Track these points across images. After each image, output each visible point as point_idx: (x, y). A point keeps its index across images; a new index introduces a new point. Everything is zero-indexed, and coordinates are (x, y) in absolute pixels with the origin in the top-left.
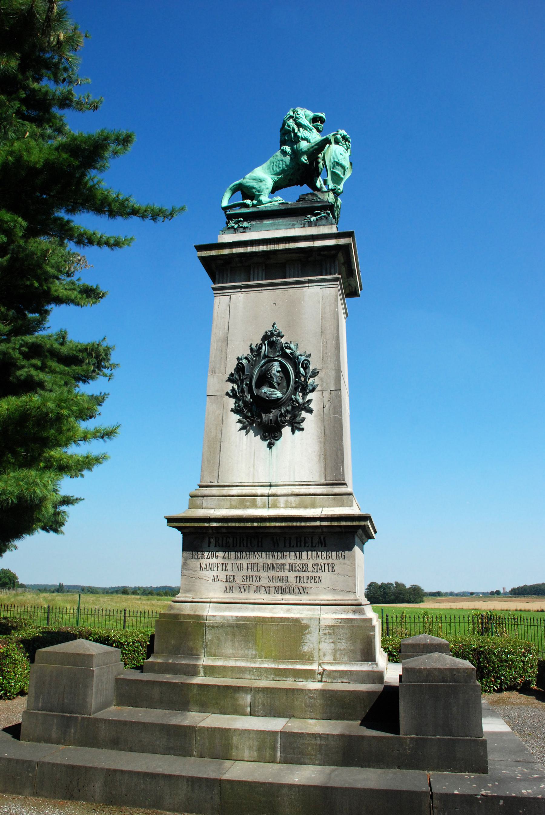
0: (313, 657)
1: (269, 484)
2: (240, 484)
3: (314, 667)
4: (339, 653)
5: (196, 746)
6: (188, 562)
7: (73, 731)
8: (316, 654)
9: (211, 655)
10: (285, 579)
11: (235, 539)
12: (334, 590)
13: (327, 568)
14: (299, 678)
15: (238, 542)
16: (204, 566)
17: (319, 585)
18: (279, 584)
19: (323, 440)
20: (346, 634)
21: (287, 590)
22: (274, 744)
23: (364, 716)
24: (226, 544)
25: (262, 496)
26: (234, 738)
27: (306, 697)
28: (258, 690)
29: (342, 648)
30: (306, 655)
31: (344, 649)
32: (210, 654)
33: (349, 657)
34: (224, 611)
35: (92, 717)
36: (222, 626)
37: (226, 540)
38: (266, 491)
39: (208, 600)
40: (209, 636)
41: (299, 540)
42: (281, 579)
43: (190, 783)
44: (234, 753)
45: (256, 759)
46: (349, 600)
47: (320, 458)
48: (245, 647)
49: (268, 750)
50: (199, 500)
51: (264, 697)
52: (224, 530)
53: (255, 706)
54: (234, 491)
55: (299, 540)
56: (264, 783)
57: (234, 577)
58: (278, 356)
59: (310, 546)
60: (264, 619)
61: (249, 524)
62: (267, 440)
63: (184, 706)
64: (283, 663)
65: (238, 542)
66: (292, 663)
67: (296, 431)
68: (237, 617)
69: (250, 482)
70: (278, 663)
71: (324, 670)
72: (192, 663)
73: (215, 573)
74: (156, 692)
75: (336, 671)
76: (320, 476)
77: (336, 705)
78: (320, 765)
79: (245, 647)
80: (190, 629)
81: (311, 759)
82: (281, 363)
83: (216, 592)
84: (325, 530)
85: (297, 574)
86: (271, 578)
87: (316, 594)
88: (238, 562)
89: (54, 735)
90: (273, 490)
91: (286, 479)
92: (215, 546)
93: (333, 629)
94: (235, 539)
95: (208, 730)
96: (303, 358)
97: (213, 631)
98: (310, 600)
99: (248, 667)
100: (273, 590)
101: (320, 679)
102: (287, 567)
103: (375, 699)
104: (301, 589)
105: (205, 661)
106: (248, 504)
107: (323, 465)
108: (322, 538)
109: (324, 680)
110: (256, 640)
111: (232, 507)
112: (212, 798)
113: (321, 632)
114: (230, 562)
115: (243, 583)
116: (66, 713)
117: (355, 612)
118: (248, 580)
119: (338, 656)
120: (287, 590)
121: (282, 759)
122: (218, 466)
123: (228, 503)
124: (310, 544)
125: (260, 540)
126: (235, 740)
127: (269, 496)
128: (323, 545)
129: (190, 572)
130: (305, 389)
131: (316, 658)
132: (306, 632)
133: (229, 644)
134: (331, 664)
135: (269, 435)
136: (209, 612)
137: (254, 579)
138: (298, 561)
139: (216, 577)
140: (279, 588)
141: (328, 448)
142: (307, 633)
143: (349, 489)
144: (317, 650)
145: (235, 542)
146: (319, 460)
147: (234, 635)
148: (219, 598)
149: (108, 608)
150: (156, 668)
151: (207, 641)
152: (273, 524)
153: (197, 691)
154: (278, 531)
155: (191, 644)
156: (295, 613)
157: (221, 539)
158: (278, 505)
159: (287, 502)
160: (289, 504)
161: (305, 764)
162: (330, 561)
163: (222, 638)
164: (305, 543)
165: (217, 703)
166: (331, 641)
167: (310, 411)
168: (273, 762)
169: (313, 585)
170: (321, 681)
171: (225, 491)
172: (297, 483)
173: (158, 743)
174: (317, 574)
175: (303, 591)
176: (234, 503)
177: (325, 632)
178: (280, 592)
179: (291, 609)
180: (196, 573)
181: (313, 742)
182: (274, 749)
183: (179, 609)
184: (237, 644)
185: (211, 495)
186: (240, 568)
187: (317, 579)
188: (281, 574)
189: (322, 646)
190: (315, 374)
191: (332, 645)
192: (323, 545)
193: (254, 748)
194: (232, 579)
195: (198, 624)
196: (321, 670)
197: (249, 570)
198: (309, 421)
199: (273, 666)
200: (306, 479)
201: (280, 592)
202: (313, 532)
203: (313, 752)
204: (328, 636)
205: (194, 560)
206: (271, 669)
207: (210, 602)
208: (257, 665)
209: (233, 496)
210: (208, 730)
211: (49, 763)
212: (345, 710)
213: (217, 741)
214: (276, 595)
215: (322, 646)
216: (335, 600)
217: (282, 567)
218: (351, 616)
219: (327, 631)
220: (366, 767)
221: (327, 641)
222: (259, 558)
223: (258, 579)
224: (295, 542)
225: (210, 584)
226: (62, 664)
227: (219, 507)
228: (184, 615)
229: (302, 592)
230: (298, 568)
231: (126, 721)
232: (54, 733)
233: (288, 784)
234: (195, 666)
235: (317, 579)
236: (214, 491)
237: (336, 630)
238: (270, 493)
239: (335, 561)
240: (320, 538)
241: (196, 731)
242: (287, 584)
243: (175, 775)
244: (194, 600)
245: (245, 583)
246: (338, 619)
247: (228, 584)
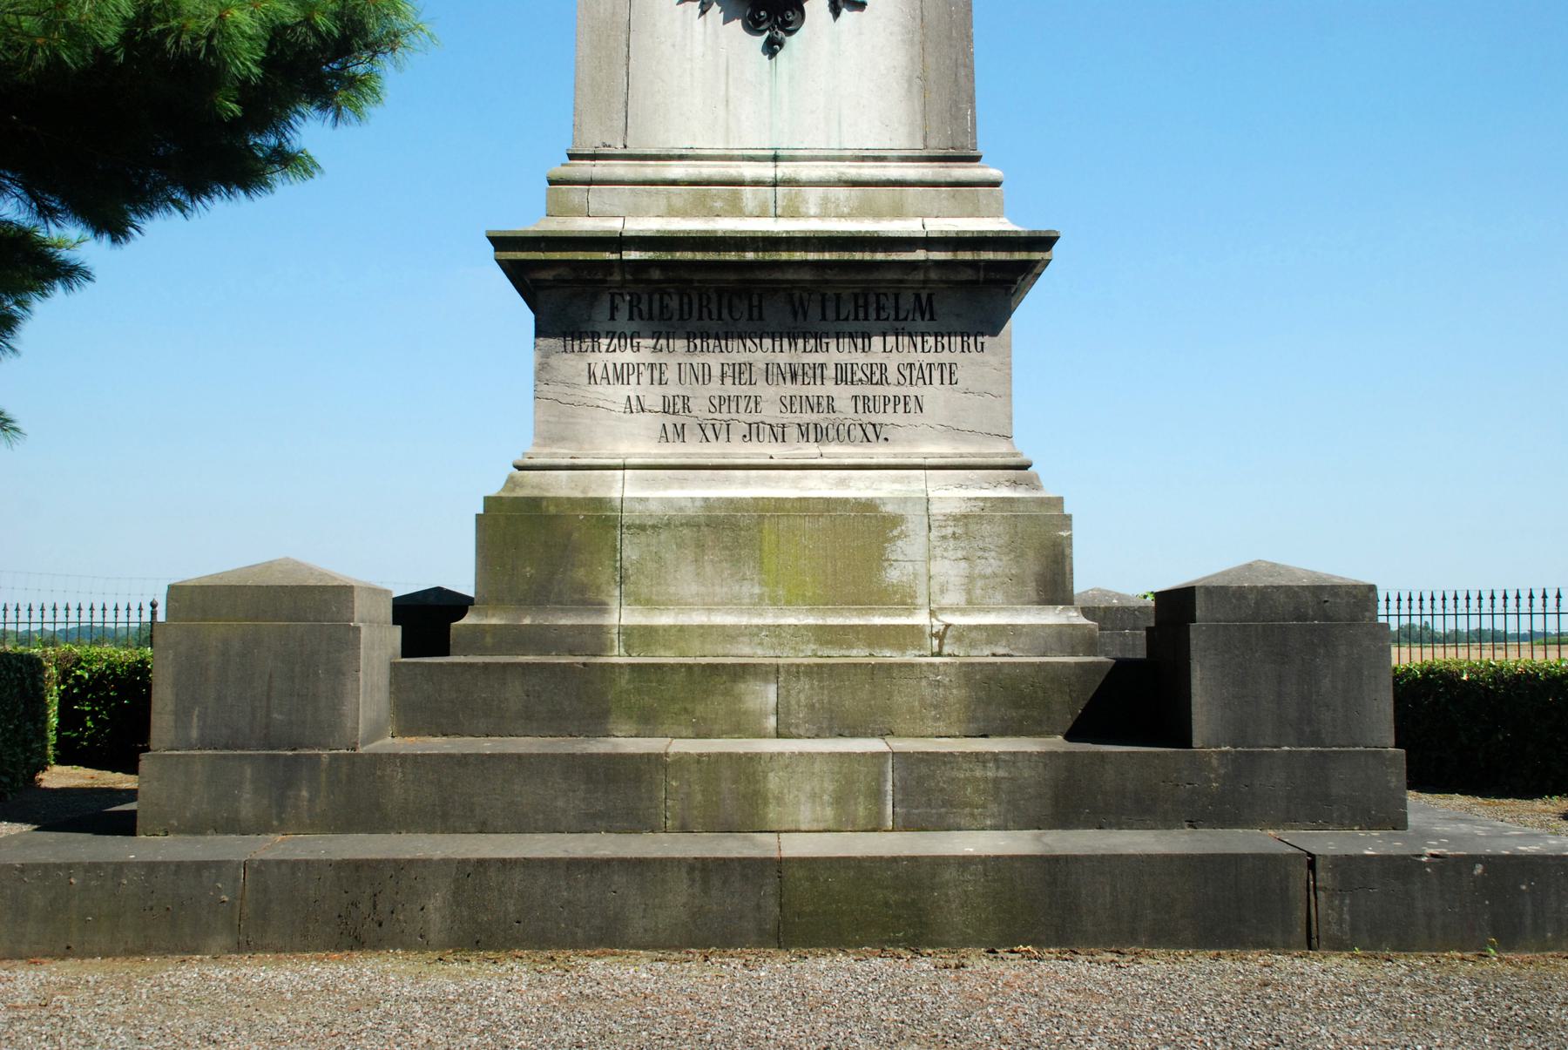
0: (913, 597)
1: (772, 153)
2: (690, 152)
3: (921, 619)
4: (980, 583)
5: (669, 803)
6: (553, 360)
7: (305, 793)
8: (921, 590)
9: (638, 601)
10: (824, 403)
11: (686, 300)
12: (954, 431)
13: (936, 374)
14: (881, 647)
15: (696, 306)
16: (599, 372)
17: (914, 417)
18: (808, 417)
19: (917, 38)
20: (999, 536)
21: (832, 433)
22: (879, 785)
23: (1070, 724)
24: (662, 313)
25: (757, 183)
26: (771, 775)
27: (924, 683)
28: (796, 671)
29: (989, 571)
30: (895, 593)
31: (995, 575)
32: (640, 601)
33: (1006, 593)
34: (666, 488)
35: (361, 750)
36: (668, 525)
37: (661, 300)
38: (766, 171)
39: (619, 461)
40: (631, 551)
41: (861, 302)
42: (813, 405)
43: (697, 874)
44: (772, 813)
45: (831, 825)
46: (997, 455)
47: (910, 85)
48: (732, 575)
49: (861, 799)
50: (576, 194)
51: (812, 688)
52: (656, 274)
53: (788, 713)
54: (676, 170)
55: (861, 302)
56: (895, 860)
57: (686, 399)
59: (892, 316)
60: (779, 503)
61: (732, 256)
62: (762, 32)
63: (596, 724)
64: (838, 613)
65: (696, 306)
66: (860, 613)
67: (844, 11)
68: (706, 500)
69: (718, 145)
70: (824, 613)
71: (948, 626)
72: (587, 622)
73: (630, 390)
74: (514, 693)
75: (978, 627)
76: (911, 135)
77: (1001, 697)
78: (995, 828)
79: (732, 575)
80: (576, 535)
81: (972, 815)
83: (637, 440)
84: (933, 275)
85: (859, 390)
86: (787, 402)
87: (910, 442)
88: (697, 360)
89: (246, 810)
90: (785, 170)
91: (816, 141)
92: (631, 318)
93: (966, 523)
94: (686, 300)
95: (699, 762)
97: (643, 538)
98: (895, 456)
99: (746, 627)
100: (792, 432)
101: (936, 649)
102: (830, 372)
103: (1099, 680)
104: (869, 430)
105: (622, 616)
106: (719, 204)
107: (918, 105)
109: (946, 650)
110: (761, 558)
111: (672, 212)
112: (758, 907)
113: (934, 533)
114: (672, 361)
115: (711, 416)
116: (278, 748)
117: (1015, 483)
118: (725, 408)
119: (979, 592)
120: (832, 433)
121: (899, 820)
122: (623, 99)
123: (663, 203)
124: (893, 314)
125: (755, 303)
126: (774, 782)
127: (775, 184)
128: (927, 316)
129: (560, 388)
132: (895, 533)
133: (687, 571)
135: (768, 19)
136: (622, 489)
137: (742, 404)
138: (860, 358)
139: (634, 402)
140: (811, 427)
141: (930, 60)
142: (899, 537)
143: (993, 173)
144: (925, 578)
145: (686, 308)
146: (909, 91)
147: (700, 546)
148: (649, 456)
150: (489, 640)
151: (626, 564)
152: (798, 256)
153: (629, 682)
154: (807, 276)
155: (580, 574)
156: (859, 487)
157: (645, 298)
158: (802, 210)
161: (959, 829)
162: (945, 357)
163: (669, 557)
164: (879, 309)
165: (686, 710)
166: (960, 554)
168: (874, 830)
169: (899, 418)
171: (651, 170)
172: (849, 153)
173: (560, 803)
174: (912, 391)
175: (873, 433)
176: (678, 202)
177: (944, 532)
178: (812, 437)
179: (850, 478)
180: (576, 391)
181: (978, 773)
182: (877, 795)
183: (538, 486)
184: (709, 569)
185: (613, 178)
186: (703, 376)
188: (814, 390)
189: (938, 567)
191: (963, 564)
192: (927, 316)
193: (826, 797)
194: (679, 405)
195: (602, 519)
196: (938, 626)
197: (728, 381)
199: (811, 621)
200: (872, 141)
201: (812, 437)
202: (901, 281)
203: (978, 799)
204: (952, 543)
205: (572, 356)
206: (807, 627)
207: (624, 467)
208: (769, 621)
209: (674, 183)
210: (699, 762)
211: (279, 863)
212: (1022, 711)
213: (725, 786)
214: (803, 444)
215: (938, 567)
216: (961, 456)
217: (818, 372)
218: (1005, 492)
219: (950, 531)
220: (1111, 826)
221: (950, 554)
222: (753, 348)
223: (752, 405)
224: (852, 307)
225: (620, 419)
226: (256, 618)
228: (557, 501)
229: (872, 436)
230: (859, 375)
231: (465, 756)
232: (247, 805)
233: (955, 857)
234: (600, 630)
235: (912, 404)
236: (620, 169)
237: (973, 527)
238: (779, 175)
240: (918, 297)
241: (666, 766)
242: (832, 416)
243: (654, 860)
244: (577, 461)
245: (717, 415)
246: (976, 499)
247: (669, 420)
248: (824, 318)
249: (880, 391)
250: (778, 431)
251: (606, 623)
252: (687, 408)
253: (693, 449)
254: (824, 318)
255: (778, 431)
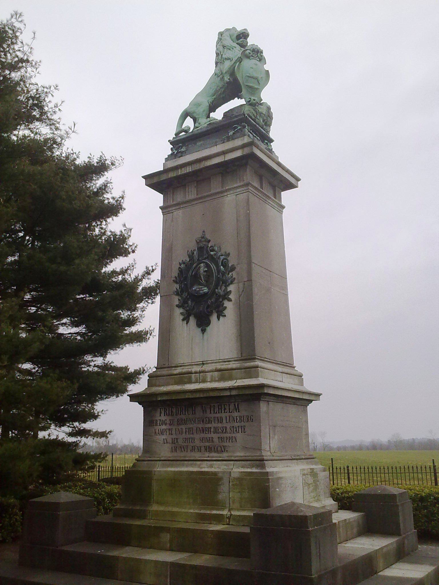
3: (225, 512)
10: (211, 439)
12: (245, 448)
16: (157, 431)
18: (207, 444)
25: (196, 373)
58: (205, 259)
73: (164, 437)
82: (207, 264)
85: (219, 435)
88: (180, 427)
91: (213, 358)
93: (240, 480)
96: (222, 258)
102: (212, 430)
104: (223, 448)
105: (155, 507)
108: (236, 405)
114: (174, 428)
117: (257, 466)
130: (227, 283)
131: (228, 505)
134: (238, 510)
137: (191, 440)
149: (398, 466)
159: (212, 376)
160: (213, 378)
164: (225, 409)
166: (238, 490)
167: (230, 300)
169: (230, 444)
170: (229, 524)
174: (234, 435)
179: (213, 464)
186: (181, 433)
187: (234, 439)
188: (209, 436)
190: (233, 269)
191: (239, 494)
198: (230, 307)
216: (245, 456)
218: (254, 470)
227: (168, 384)
235: (234, 439)
239: (246, 424)
248: (211, 413)
249: (225, 435)
250: (199, 448)
251: (147, 509)
252: (177, 442)
253: (180, 455)
254: (211, 413)
255: (199, 448)
